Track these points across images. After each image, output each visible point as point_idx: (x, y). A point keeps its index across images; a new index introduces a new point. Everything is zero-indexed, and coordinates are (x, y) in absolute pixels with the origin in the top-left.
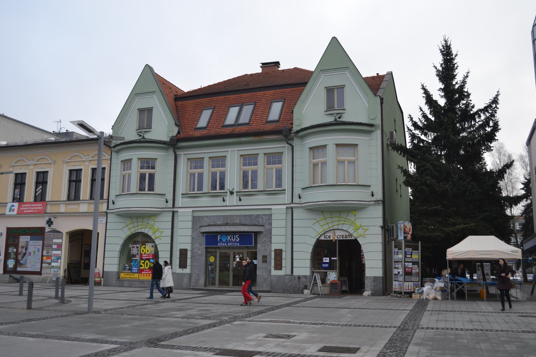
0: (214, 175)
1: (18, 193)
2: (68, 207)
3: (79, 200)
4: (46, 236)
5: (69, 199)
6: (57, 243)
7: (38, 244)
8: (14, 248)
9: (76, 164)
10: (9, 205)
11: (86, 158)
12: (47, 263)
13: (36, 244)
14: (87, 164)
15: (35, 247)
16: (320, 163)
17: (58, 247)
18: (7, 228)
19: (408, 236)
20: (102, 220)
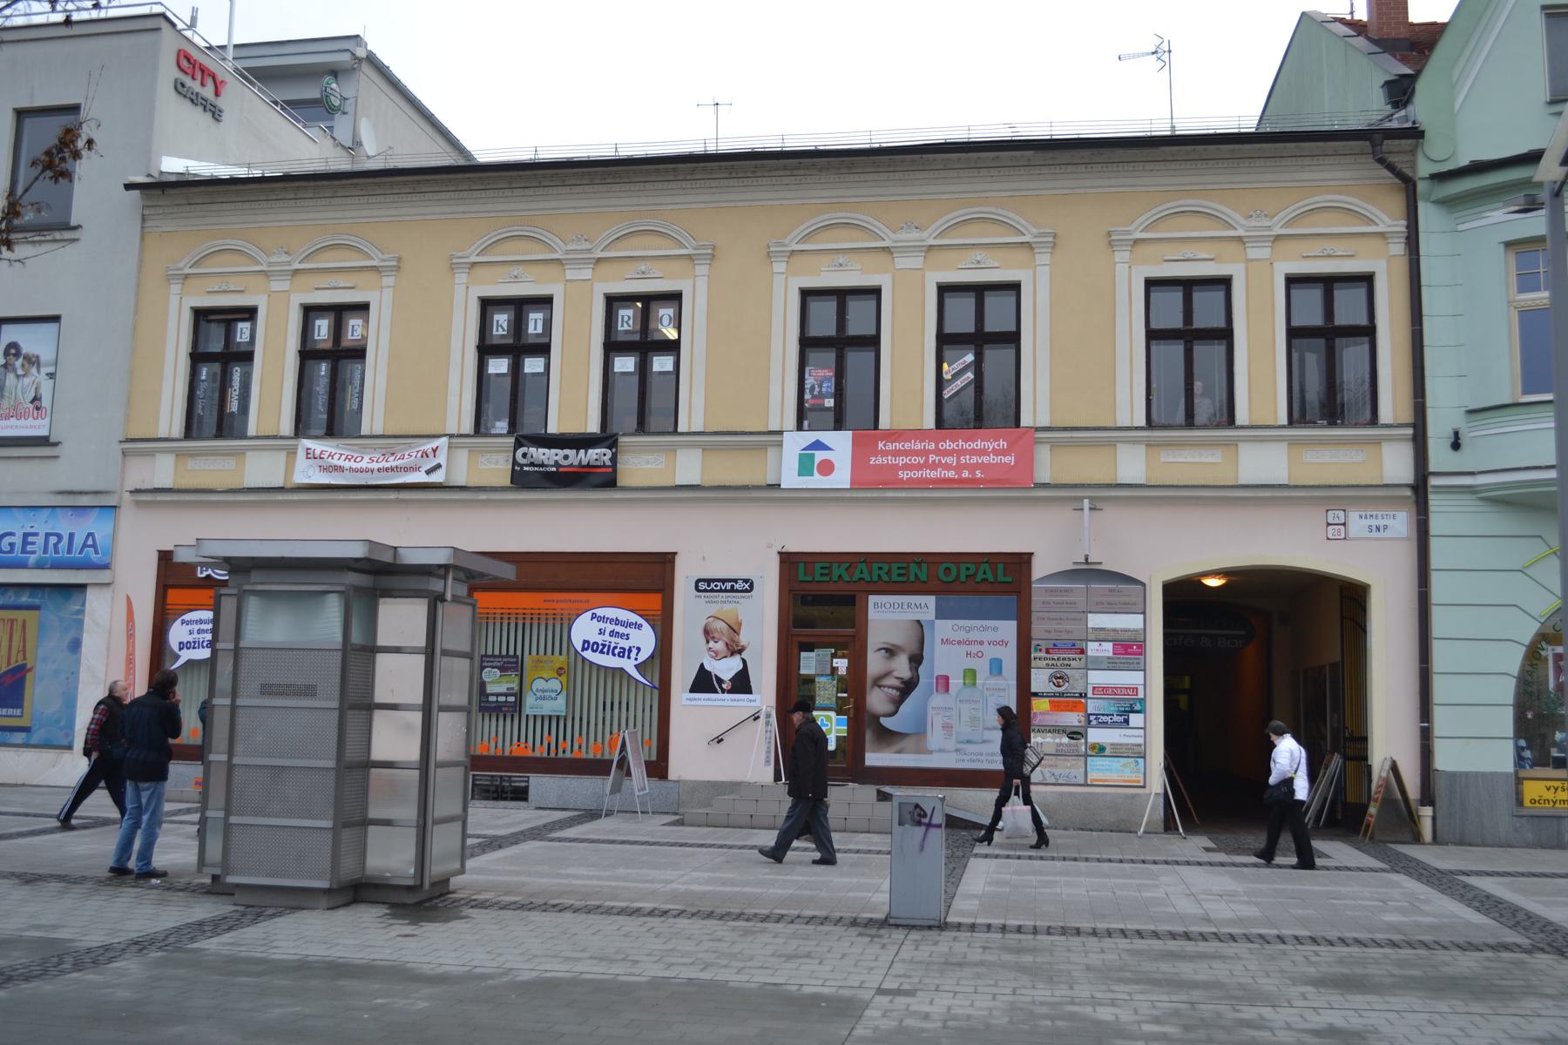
1: (829, 387)
2: (1163, 459)
3: (243, 436)
4: (1037, 600)
5: (189, 433)
6: (1115, 630)
7: (997, 637)
8: (834, 656)
9: (342, 280)
10: (796, 442)
11: (1253, 223)
12: (1057, 730)
13: (973, 636)
14: (276, 286)
15: (975, 649)
17: (1120, 650)
18: (780, 553)
20: (1381, 523)
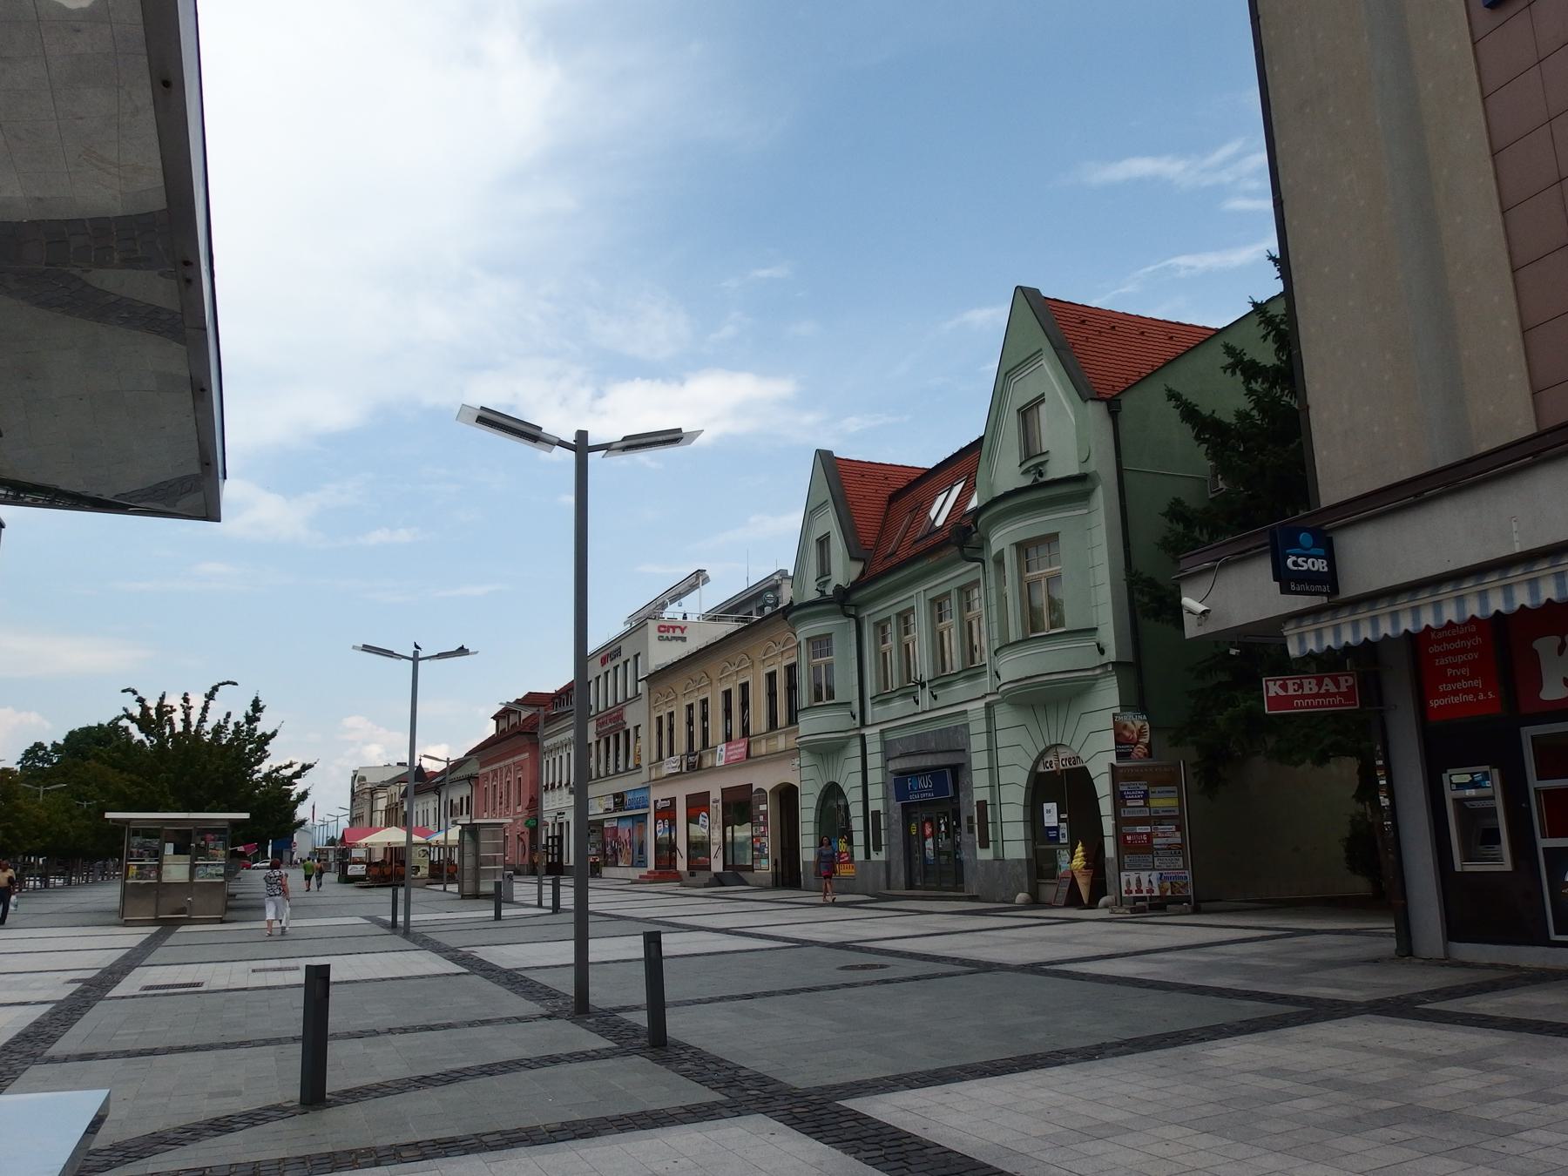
0: (816, 669)
2: (772, 744)
16: (1043, 579)
19: (1136, 750)
